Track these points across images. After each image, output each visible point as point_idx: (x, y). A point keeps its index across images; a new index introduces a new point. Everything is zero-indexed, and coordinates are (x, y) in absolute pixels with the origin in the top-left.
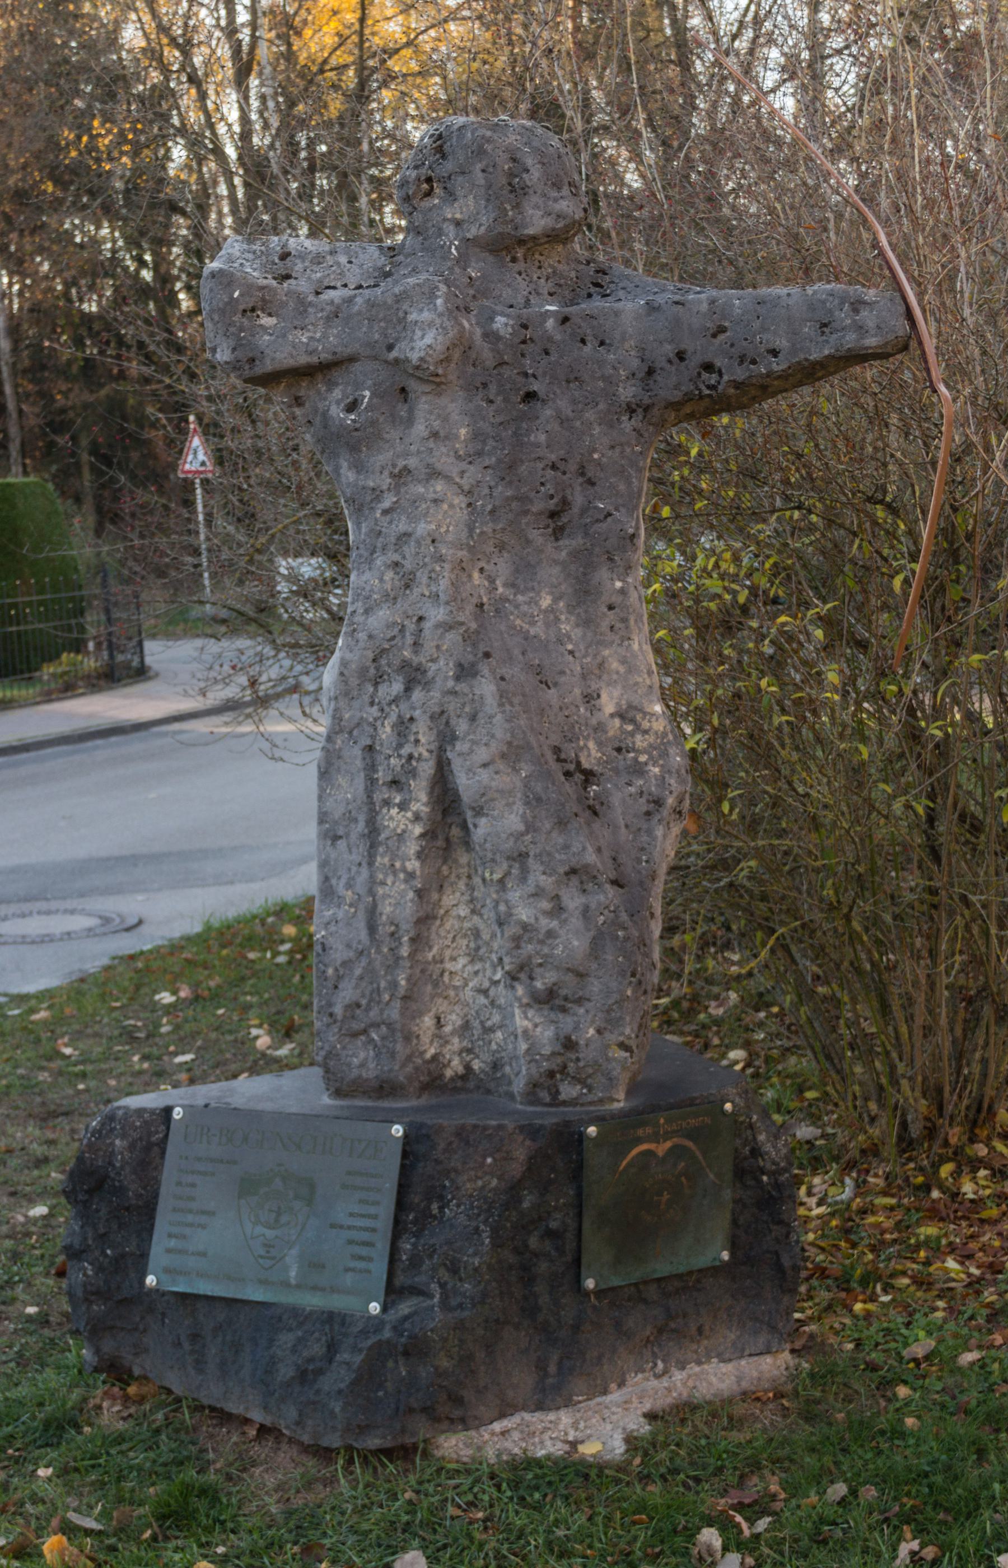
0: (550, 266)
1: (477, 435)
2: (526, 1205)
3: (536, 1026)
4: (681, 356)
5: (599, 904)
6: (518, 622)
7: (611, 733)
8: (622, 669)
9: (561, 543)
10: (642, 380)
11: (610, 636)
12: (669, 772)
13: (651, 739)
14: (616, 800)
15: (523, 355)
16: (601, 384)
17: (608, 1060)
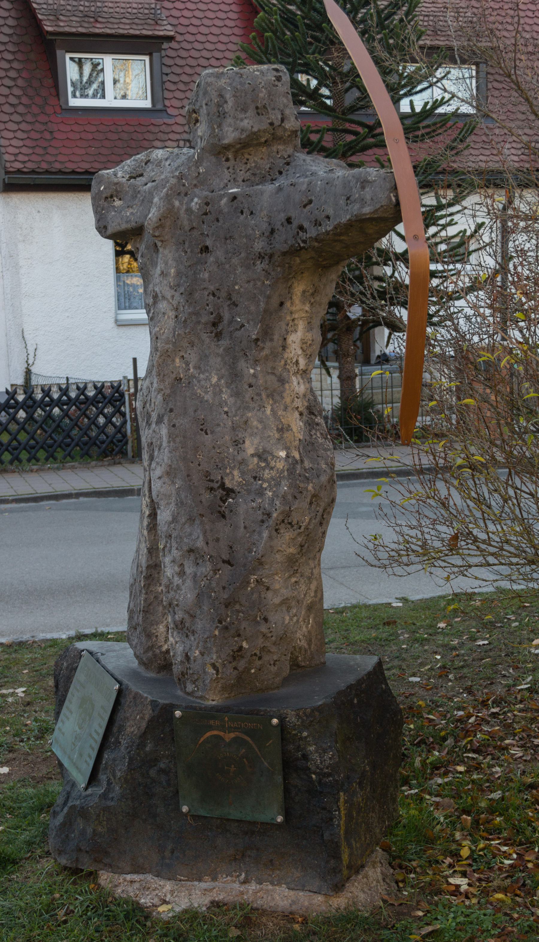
0: (255, 161)
1: (179, 274)
2: (148, 749)
3: (176, 642)
4: (289, 221)
5: (202, 573)
6: (199, 391)
7: (251, 467)
8: (260, 426)
9: (220, 343)
10: (268, 237)
11: (252, 405)
12: (277, 496)
13: (273, 473)
14: (242, 510)
15: (203, 222)
16: (245, 240)
17: (205, 672)
